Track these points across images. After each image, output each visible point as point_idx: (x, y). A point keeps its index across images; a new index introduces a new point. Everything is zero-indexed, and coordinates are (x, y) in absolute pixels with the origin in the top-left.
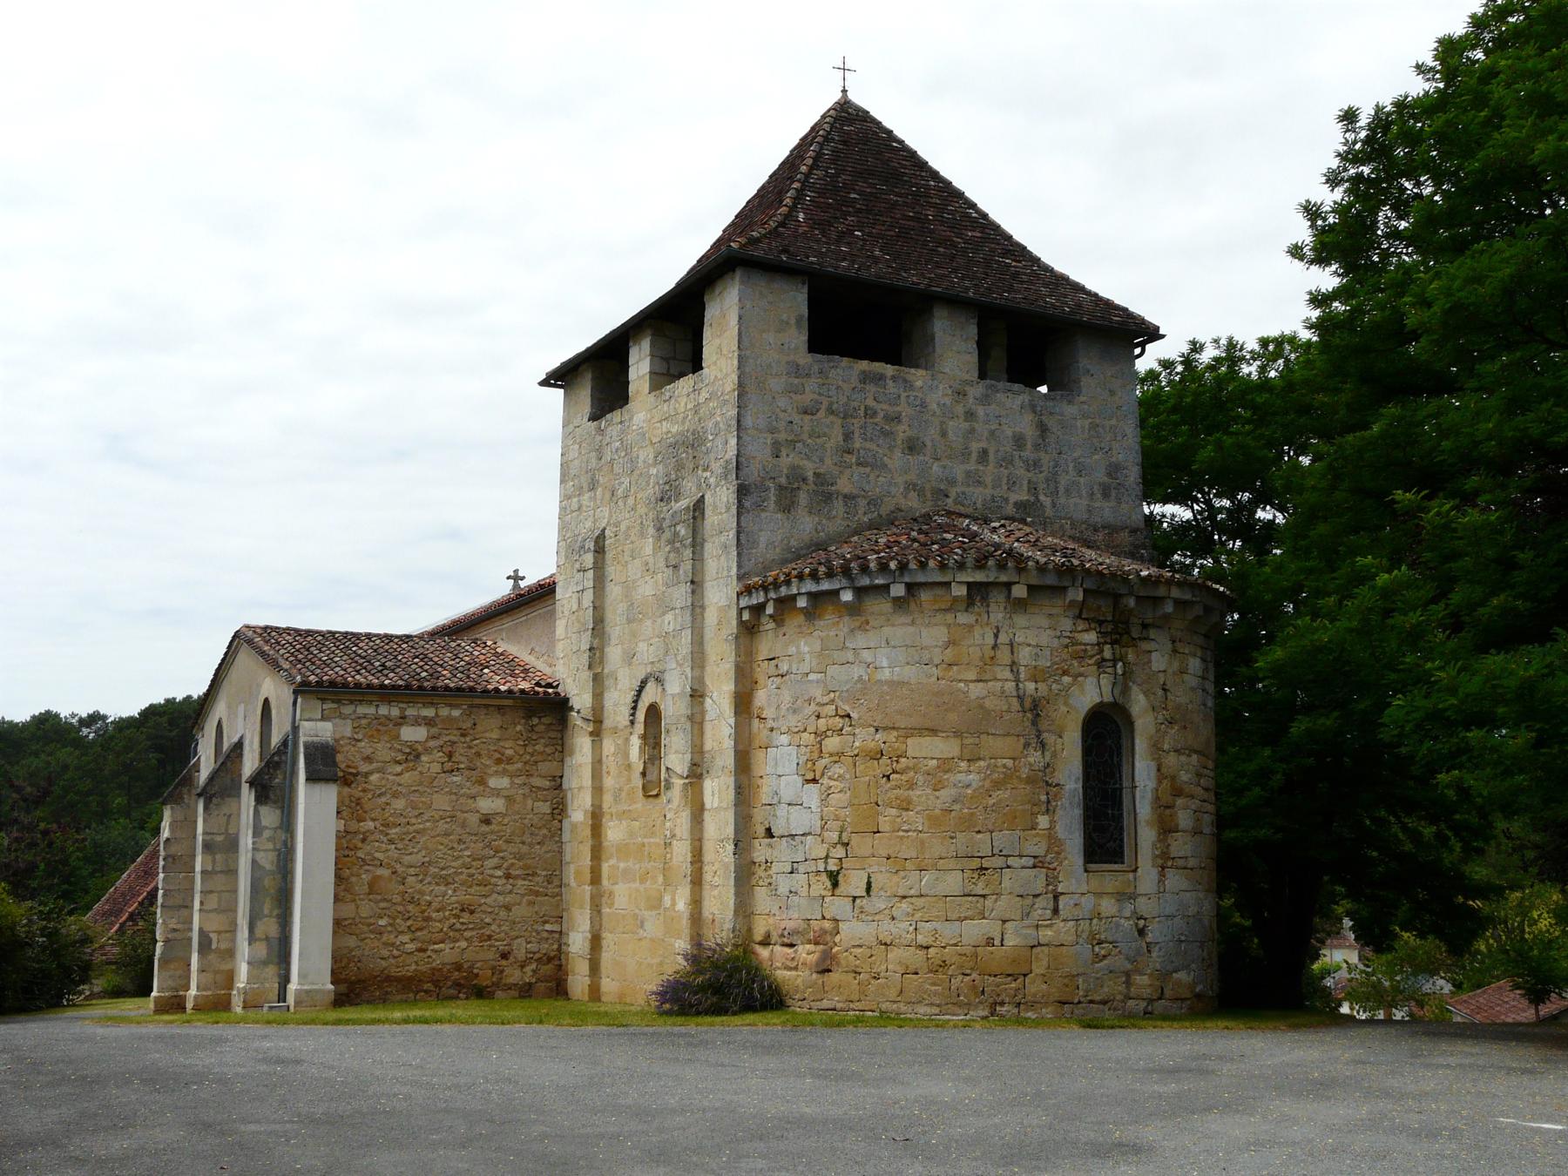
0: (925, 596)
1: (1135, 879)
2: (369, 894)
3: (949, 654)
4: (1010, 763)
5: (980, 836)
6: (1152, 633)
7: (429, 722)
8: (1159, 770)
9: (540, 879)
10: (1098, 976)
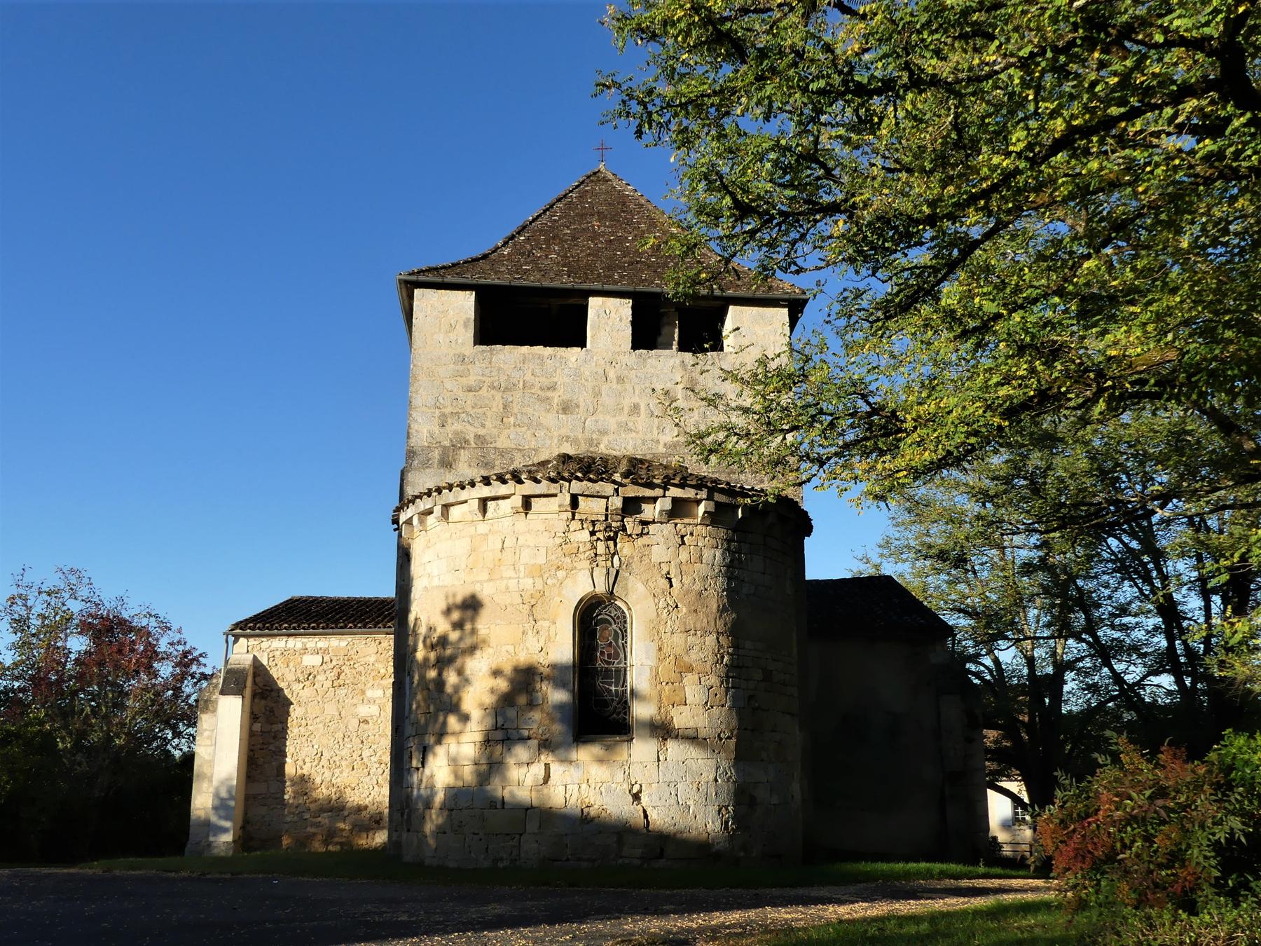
8: (660, 649)
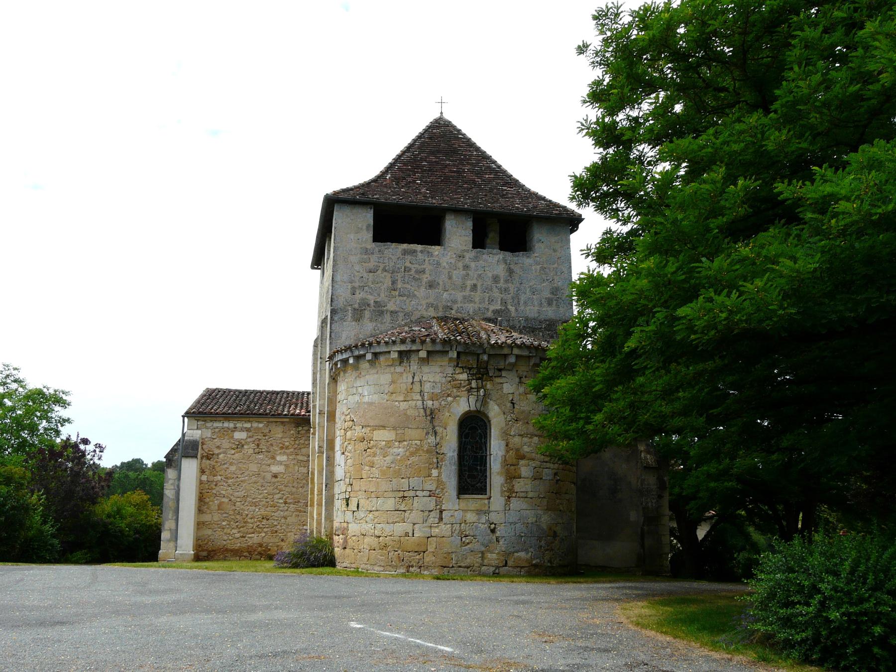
0: (382, 358)
1: (489, 503)
2: (218, 510)
3: (391, 389)
4: (418, 442)
5: (403, 480)
6: (504, 373)
7: (248, 430)
8: (507, 445)
9: (302, 504)
10: (465, 553)
